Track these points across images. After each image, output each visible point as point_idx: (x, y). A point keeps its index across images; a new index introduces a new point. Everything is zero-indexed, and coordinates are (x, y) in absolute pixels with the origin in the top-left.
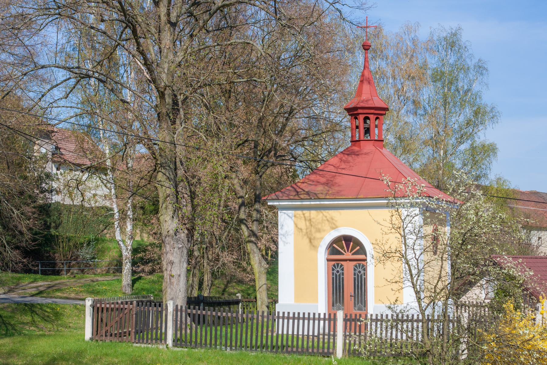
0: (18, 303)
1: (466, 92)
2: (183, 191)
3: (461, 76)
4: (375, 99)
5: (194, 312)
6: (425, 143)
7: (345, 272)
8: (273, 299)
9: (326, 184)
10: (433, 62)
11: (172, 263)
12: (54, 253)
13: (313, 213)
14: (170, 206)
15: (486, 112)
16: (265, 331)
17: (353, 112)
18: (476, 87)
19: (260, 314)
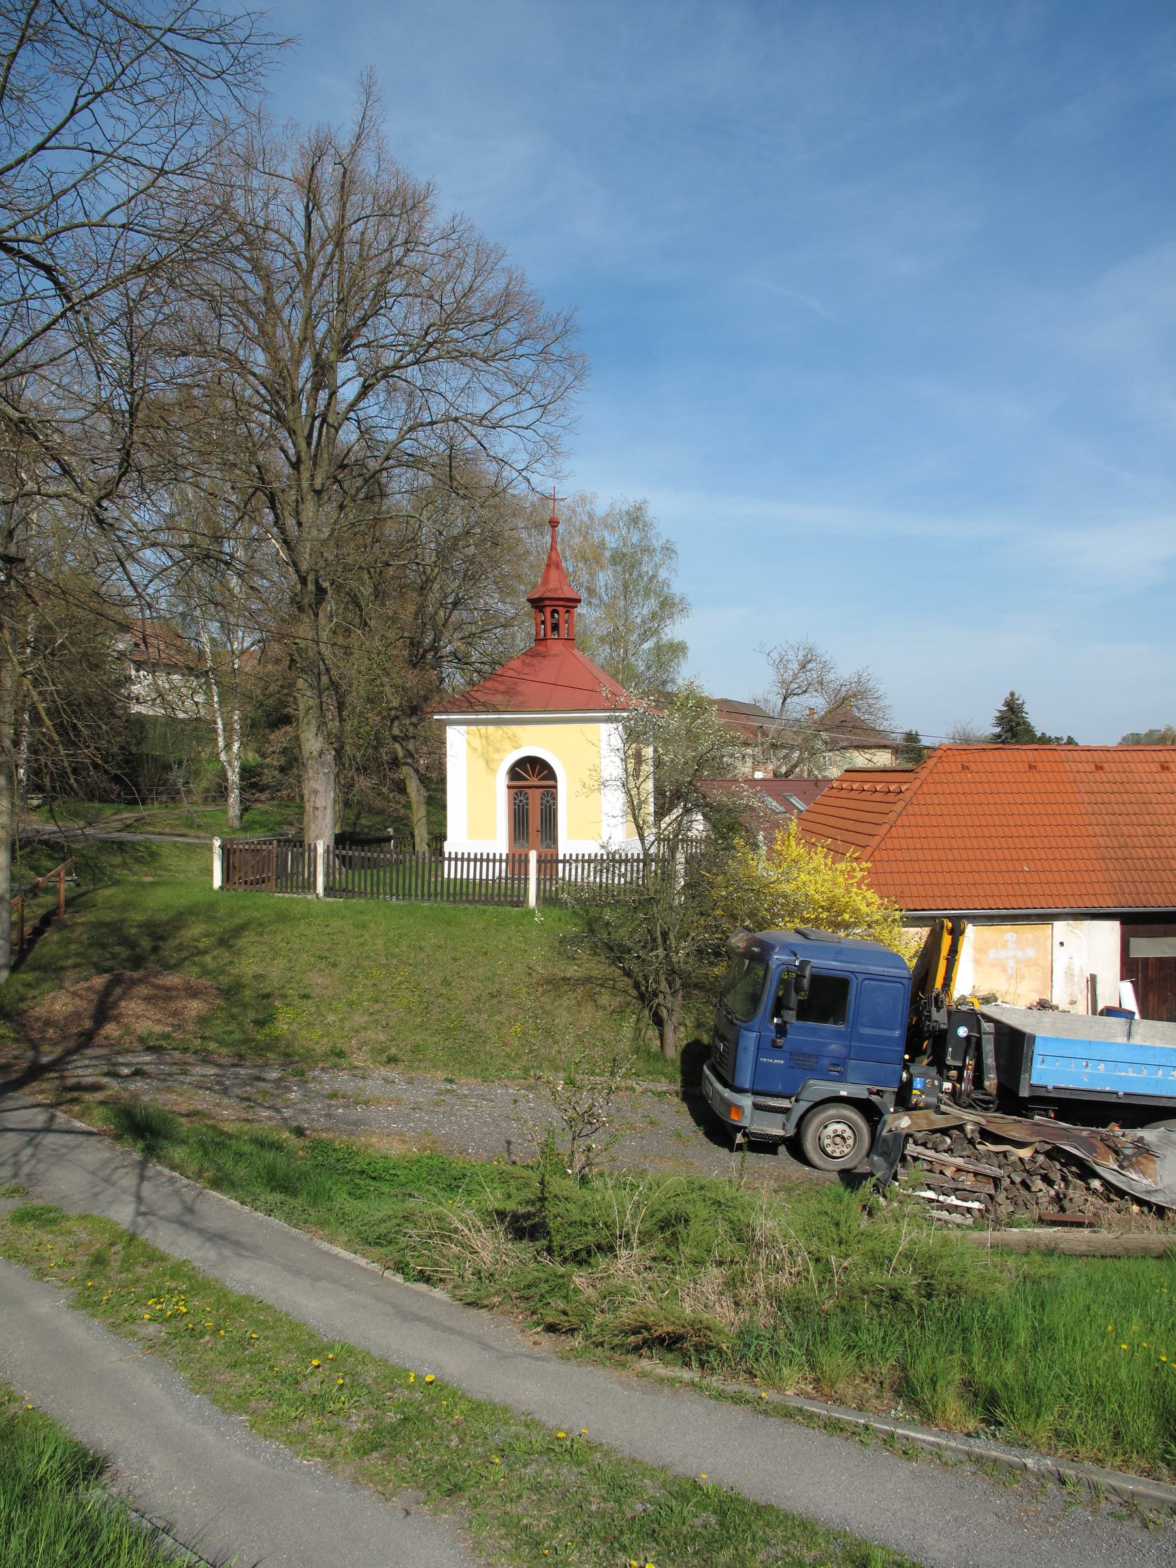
0: (104, 841)
1: (651, 579)
2: (329, 701)
3: (646, 559)
4: (565, 587)
5: (344, 852)
6: (602, 640)
7: (530, 801)
8: (439, 837)
9: (507, 693)
10: (612, 541)
11: (316, 792)
12: (137, 777)
13: (491, 728)
14: (313, 721)
15: (674, 603)
16: (426, 875)
17: (538, 604)
18: (663, 574)
19: (420, 856)
